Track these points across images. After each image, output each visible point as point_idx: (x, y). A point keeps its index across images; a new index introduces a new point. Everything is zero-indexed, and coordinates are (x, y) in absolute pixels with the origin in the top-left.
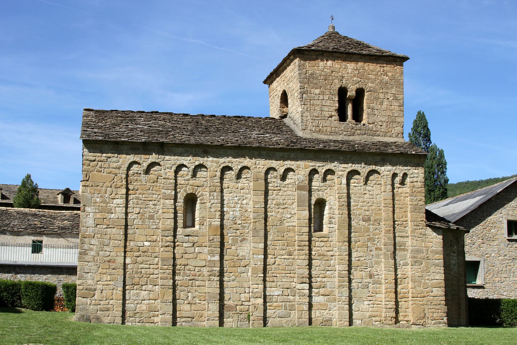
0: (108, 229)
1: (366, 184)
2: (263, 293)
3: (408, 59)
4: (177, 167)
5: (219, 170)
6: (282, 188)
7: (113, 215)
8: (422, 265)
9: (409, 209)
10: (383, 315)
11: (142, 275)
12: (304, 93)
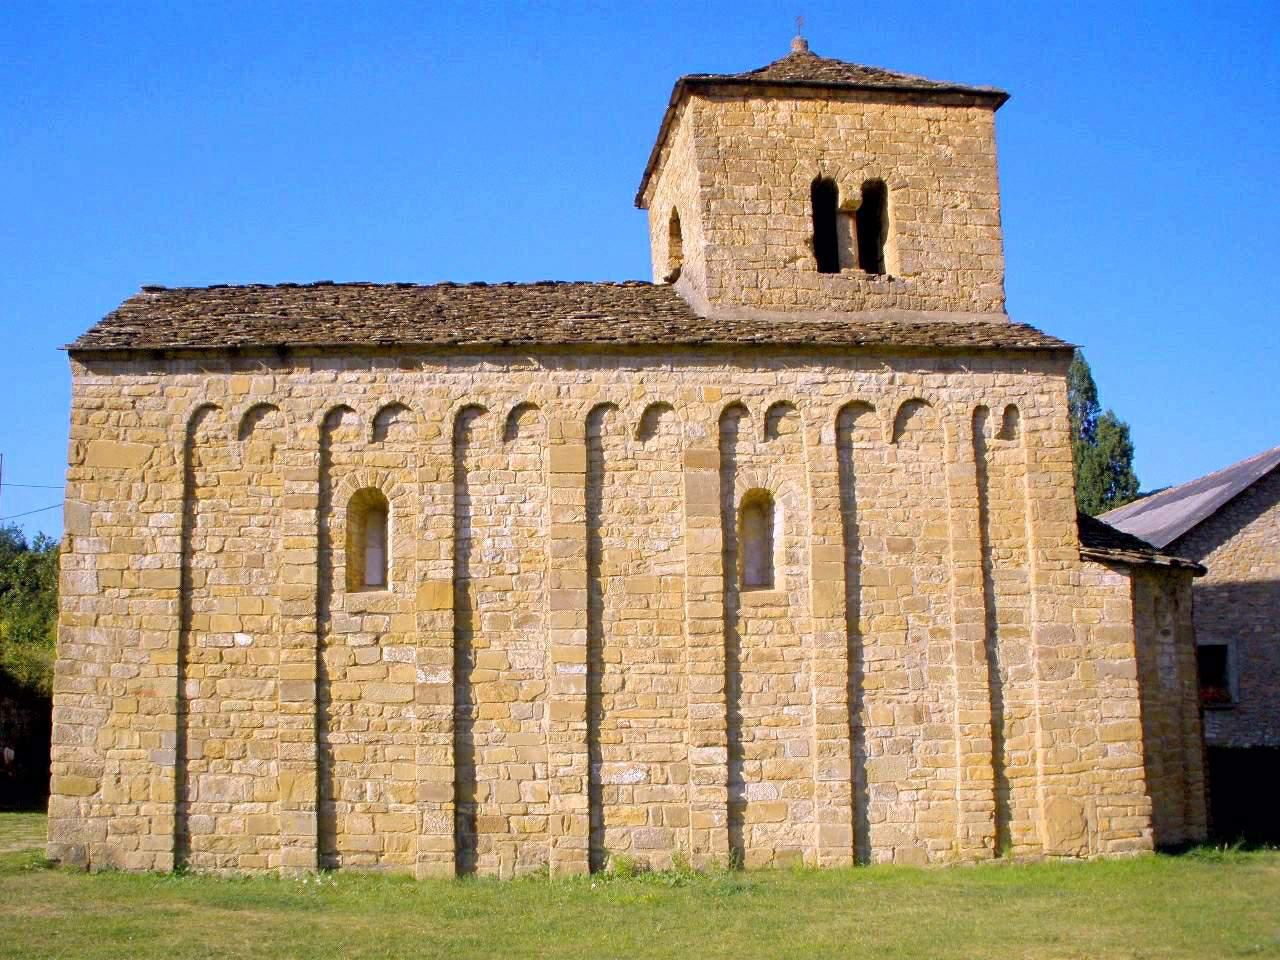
1: (894, 441)
2: (586, 779)
4: (328, 416)
7: (149, 557)
8: (1074, 677)
9: (1028, 511)
11: (229, 730)
12: (714, 197)
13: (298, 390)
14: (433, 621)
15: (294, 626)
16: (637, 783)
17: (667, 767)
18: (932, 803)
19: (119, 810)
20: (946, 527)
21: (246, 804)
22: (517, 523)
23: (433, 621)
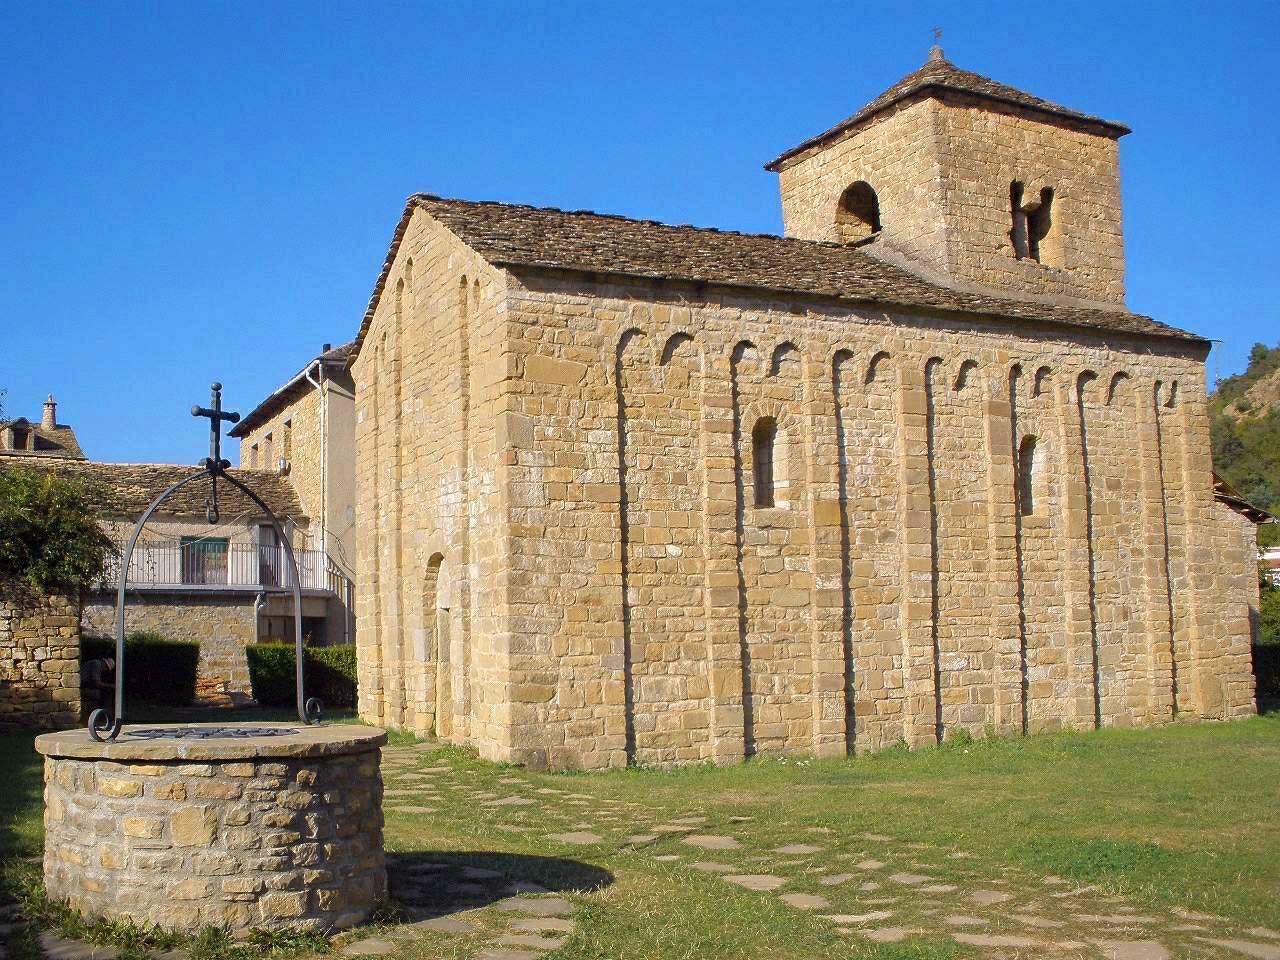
0: (578, 513)
3: (1128, 131)
5: (829, 357)
6: (955, 408)
10: (1150, 703)
19: (574, 714)
20: (1139, 471)
21: (681, 702)
22: (877, 454)
23: (826, 535)
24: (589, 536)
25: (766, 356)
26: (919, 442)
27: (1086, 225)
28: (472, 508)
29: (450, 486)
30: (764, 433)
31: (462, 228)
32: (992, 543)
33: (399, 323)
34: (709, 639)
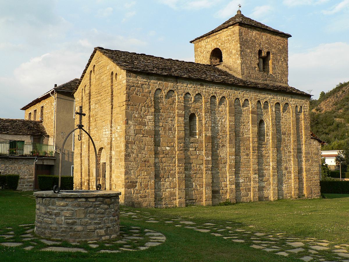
12: (242, 51)
13: (179, 87)
14: (208, 145)
15: (180, 146)
16: (242, 182)
17: (247, 179)
18: (288, 187)
19: (141, 192)
20: (291, 130)
21: (169, 189)
22: (221, 124)
23: (208, 145)
24: (146, 144)
25: (193, 97)
26: (232, 121)
27: (278, 62)
28: (113, 136)
29: (107, 129)
30: (192, 117)
31: (111, 58)
32: (251, 148)
33: (90, 83)
34: (177, 172)
